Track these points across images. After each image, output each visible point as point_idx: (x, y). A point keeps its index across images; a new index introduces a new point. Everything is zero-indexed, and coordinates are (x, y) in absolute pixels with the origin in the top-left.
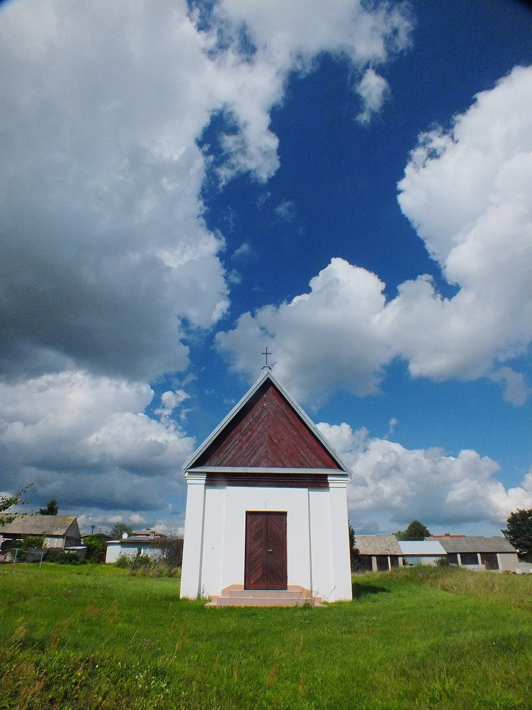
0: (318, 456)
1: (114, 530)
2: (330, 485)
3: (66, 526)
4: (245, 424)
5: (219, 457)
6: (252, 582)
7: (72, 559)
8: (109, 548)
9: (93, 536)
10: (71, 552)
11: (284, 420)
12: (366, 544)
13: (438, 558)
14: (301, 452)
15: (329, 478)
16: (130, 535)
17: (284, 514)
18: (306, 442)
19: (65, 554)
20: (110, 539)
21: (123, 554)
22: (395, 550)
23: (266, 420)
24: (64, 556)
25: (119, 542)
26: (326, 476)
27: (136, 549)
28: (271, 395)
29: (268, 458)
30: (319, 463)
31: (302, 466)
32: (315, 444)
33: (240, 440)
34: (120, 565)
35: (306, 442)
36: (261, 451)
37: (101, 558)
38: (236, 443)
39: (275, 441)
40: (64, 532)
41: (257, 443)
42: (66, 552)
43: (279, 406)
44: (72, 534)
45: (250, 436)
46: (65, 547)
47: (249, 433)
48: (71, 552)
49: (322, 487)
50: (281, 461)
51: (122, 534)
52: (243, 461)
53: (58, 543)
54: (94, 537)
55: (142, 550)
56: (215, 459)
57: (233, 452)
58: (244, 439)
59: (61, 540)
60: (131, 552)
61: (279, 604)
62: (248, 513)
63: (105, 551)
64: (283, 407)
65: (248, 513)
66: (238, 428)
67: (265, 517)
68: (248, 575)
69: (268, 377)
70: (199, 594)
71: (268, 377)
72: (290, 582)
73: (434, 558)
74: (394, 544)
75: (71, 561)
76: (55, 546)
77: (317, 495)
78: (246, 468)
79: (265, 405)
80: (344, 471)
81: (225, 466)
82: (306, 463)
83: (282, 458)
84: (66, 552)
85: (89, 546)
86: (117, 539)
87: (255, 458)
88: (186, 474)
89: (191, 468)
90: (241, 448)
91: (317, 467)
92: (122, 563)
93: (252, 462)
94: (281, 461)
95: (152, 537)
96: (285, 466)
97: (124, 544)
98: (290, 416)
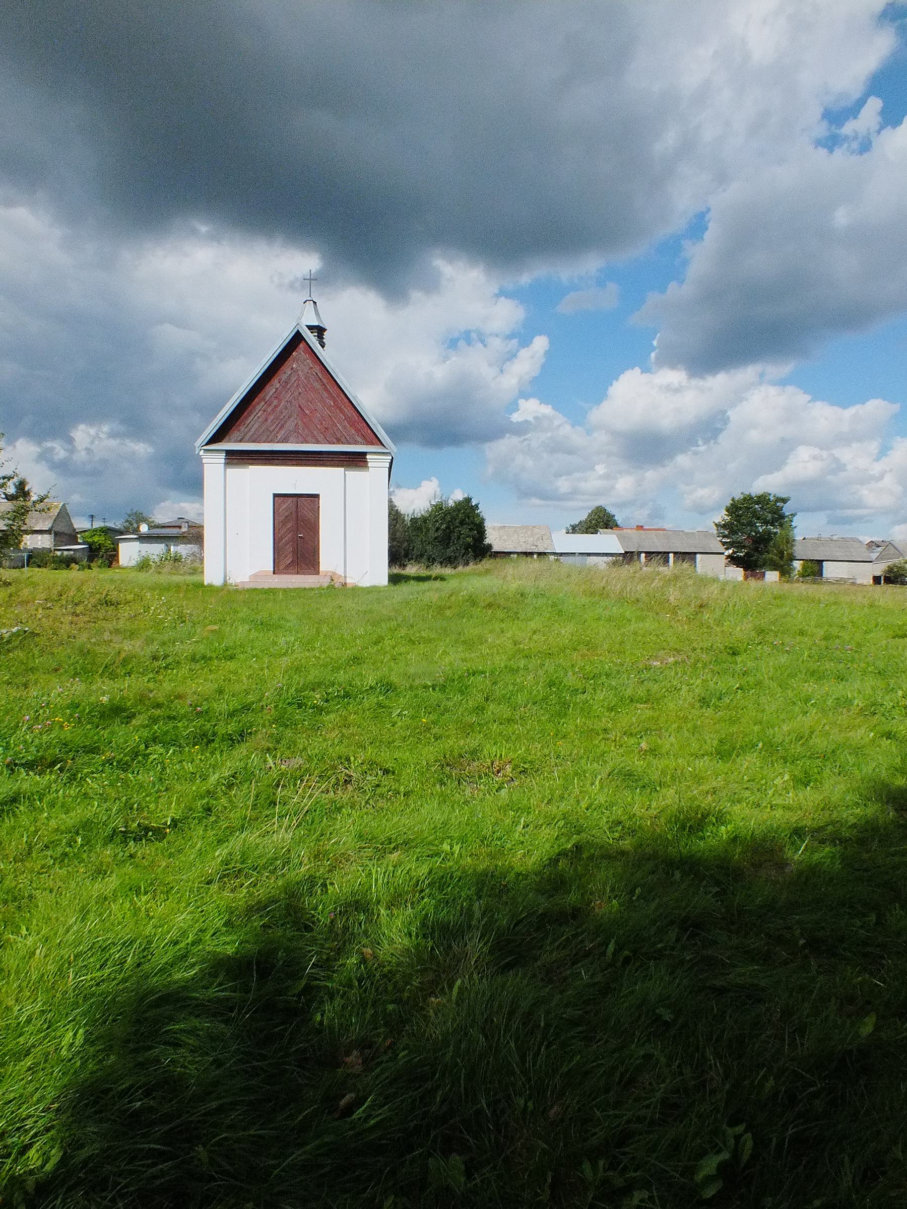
0: (358, 431)
1: (127, 521)
2: (370, 464)
3: (50, 517)
4: (270, 390)
5: (239, 431)
6: (281, 568)
7: (67, 563)
8: (122, 547)
9: (95, 530)
10: (65, 553)
11: (317, 385)
12: (505, 537)
13: (610, 558)
14: (338, 425)
15: (368, 457)
16: (150, 527)
17: (317, 496)
18: (344, 413)
19: (57, 556)
20: (122, 533)
21: (144, 554)
22: (545, 546)
23: (295, 385)
24: (56, 559)
25: (136, 537)
26: (365, 454)
27: (162, 546)
28: (302, 353)
29: (298, 433)
30: (359, 439)
31: (339, 441)
32: (355, 415)
33: (264, 411)
34: (142, 568)
35: (344, 413)
36: (290, 425)
37: (112, 558)
38: (259, 415)
39: (307, 412)
40: (50, 525)
41: (284, 414)
42: (59, 553)
43: (312, 368)
44: (60, 528)
45: (276, 407)
46: (55, 546)
47: (275, 402)
48: (65, 553)
49: (360, 466)
50: (314, 436)
51: (138, 527)
52: (268, 436)
53: (44, 542)
54: (96, 531)
55: (172, 547)
56: (235, 434)
57: (256, 426)
58: (269, 409)
59: (46, 536)
60: (155, 550)
61: (303, 586)
62: (276, 496)
63: (116, 550)
64: (317, 369)
65: (275, 496)
66: (261, 395)
67: (295, 499)
68: (276, 561)
69: (298, 331)
70: (225, 581)
71: (298, 331)
72: (323, 567)
73: (605, 558)
74: (545, 537)
75: (68, 566)
76: (39, 545)
77: (354, 475)
78: (272, 444)
79: (294, 366)
80: (383, 445)
81: (248, 441)
82: (343, 439)
83: (315, 433)
84: (59, 553)
85: (91, 545)
86: (133, 534)
87: (283, 432)
88: (202, 453)
89: (206, 444)
90: (266, 420)
91: (356, 443)
92: (144, 565)
93: (279, 438)
94: (314, 436)
95: (184, 530)
96: (318, 442)
97: (144, 539)
98: (325, 381)
